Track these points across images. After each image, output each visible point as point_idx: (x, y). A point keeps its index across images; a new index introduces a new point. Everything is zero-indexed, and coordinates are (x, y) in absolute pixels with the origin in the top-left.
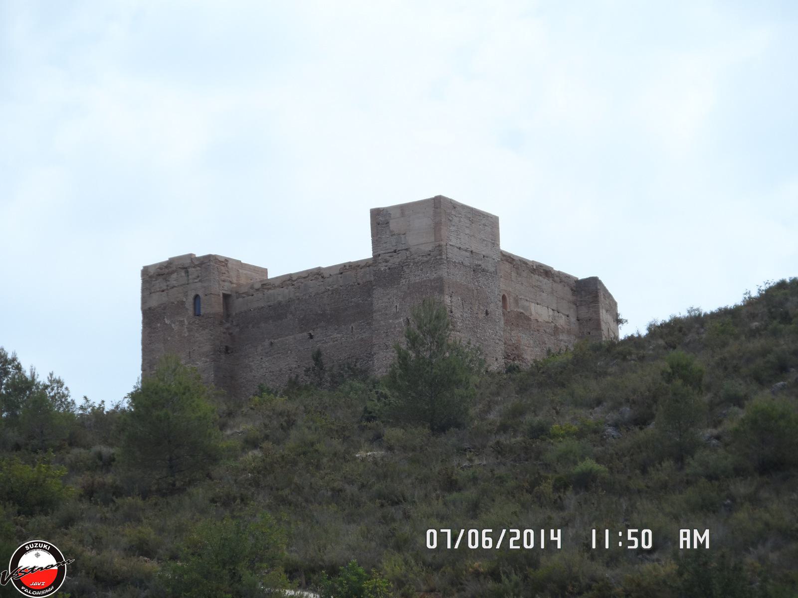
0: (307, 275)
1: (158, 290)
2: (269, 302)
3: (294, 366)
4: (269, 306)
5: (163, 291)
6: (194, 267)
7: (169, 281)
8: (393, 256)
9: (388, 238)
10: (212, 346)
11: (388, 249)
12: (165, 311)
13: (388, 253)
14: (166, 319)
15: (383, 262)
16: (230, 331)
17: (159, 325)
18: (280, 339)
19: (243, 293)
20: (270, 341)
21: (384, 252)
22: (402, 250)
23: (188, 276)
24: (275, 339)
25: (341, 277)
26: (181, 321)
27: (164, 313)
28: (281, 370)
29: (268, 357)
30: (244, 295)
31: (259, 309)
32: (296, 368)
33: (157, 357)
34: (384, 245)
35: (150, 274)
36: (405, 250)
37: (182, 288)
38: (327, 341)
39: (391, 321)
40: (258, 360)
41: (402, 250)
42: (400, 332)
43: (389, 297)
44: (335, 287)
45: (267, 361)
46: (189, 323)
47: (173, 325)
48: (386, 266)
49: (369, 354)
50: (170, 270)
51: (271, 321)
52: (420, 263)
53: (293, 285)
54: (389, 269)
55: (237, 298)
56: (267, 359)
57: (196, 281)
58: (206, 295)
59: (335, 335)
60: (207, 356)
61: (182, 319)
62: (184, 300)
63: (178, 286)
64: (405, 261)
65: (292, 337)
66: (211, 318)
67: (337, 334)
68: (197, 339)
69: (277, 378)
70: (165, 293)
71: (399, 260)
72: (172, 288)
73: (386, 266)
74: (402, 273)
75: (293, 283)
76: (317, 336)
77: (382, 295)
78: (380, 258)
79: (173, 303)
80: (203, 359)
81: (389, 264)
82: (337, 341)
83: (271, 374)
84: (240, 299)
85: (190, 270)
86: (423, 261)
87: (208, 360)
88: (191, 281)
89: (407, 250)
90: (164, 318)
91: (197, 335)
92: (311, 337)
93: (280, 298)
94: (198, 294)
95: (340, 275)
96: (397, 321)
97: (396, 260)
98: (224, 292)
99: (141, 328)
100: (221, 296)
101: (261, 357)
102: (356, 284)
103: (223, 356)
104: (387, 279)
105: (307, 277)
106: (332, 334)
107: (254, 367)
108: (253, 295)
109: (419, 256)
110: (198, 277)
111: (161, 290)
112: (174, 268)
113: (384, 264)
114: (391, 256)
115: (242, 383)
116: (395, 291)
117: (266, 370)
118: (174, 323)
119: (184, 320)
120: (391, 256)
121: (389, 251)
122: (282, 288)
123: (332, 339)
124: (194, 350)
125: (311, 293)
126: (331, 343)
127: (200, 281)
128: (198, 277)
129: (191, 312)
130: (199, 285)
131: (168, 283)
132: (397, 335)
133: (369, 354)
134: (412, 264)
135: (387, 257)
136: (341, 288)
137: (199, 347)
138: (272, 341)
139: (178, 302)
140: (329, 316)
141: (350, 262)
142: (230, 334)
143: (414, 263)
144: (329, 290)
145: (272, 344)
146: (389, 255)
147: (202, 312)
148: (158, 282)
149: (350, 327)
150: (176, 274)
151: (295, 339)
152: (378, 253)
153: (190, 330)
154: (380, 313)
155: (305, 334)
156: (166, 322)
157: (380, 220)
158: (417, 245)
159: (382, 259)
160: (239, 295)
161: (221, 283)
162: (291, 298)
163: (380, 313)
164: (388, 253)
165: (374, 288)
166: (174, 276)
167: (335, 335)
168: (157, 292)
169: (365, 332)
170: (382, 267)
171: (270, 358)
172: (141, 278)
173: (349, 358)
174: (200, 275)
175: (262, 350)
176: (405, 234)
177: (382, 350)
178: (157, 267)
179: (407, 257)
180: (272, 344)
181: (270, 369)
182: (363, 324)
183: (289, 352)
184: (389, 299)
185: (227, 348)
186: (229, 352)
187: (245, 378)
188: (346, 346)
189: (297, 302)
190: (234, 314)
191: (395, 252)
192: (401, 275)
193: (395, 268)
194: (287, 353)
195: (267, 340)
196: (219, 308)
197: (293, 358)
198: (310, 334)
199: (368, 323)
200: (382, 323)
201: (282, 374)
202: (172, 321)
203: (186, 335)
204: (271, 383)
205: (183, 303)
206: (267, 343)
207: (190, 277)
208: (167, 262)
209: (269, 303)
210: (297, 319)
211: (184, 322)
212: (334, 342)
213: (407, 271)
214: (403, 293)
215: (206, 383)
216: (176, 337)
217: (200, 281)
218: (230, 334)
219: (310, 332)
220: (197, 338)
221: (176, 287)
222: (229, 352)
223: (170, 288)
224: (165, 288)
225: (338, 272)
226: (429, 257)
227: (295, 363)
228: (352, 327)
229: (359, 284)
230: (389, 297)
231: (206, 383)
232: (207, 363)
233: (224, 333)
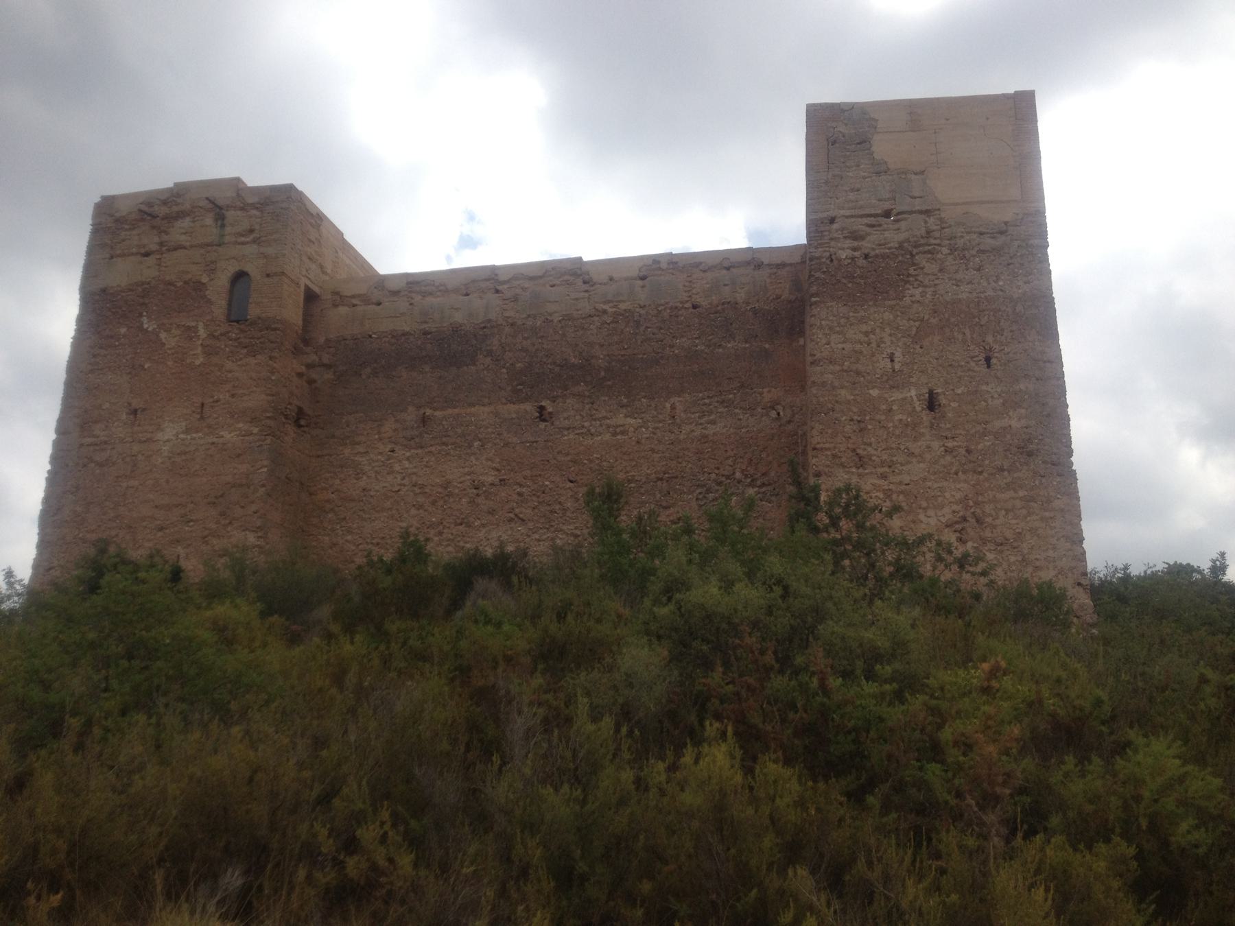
0: (540, 274)
1: (134, 250)
2: (426, 322)
3: (490, 479)
4: (426, 333)
5: (147, 255)
6: (242, 209)
7: (166, 233)
8: (880, 225)
9: (864, 178)
10: (270, 398)
11: (861, 207)
12: (147, 301)
13: (862, 216)
14: (145, 320)
15: (845, 237)
16: (314, 376)
17: (123, 330)
18: (450, 411)
19: (353, 297)
20: (422, 412)
21: (848, 213)
22: (911, 212)
23: (223, 226)
24: (435, 409)
25: (643, 287)
26: (189, 328)
27: (143, 304)
28: (446, 485)
29: (410, 448)
30: (355, 301)
31: (393, 337)
32: (492, 484)
33: (107, 405)
34: (852, 196)
35: (118, 215)
36: (921, 212)
37: (202, 251)
38: (593, 430)
39: (875, 393)
40: (381, 453)
41: (911, 212)
42: (907, 425)
43: (864, 328)
44: (623, 306)
45: (408, 459)
46: (212, 336)
47: (163, 335)
48: (854, 249)
49: (728, 477)
50: (175, 209)
51: (427, 368)
52: (974, 252)
53: (497, 291)
54: (866, 256)
55: (335, 306)
56: (408, 454)
57: (243, 239)
58: (268, 275)
59: (620, 419)
60: (253, 420)
61: (193, 324)
62: (205, 279)
63: (191, 246)
64: (922, 241)
65: (486, 409)
66: (275, 329)
67: (626, 416)
68: (230, 375)
69: (434, 503)
70: (151, 260)
71: (902, 236)
72: (175, 249)
73: (854, 249)
74: (912, 271)
75: (499, 288)
76: (565, 415)
77: (843, 321)
78: (835, 226)
79: (170, 283)
80: (241, 425)
81: (866, 245)
82: (622, 433)
83: (418, 491)
84: (343, 310)
85: (230, 215)
86: (982, 247)
87: (255, 430)
88: (227, 239)
89: (927, 212)
90: (141, 315)
91: (229, 365)
92: (542, 414)
93: (458, 318)
94: (246, 269)
95: (640, 283)
96: (897, 395)
97: (892, 235)
98: (309, 283)
99: (72, 333)
100: (303, 288)
101: (390, 447)
102: (688, 305)
103: (290, 429)
104: (859, 280)
105: (541, 277)
106: (609, 415)
107: (367, 468)
108: (379, 304)
109: (968, 233)
110: (252, 231)
111: (143, 251)
112: (187, 206)
113: (849, 243)
114: (872, 226)
115: (328, 501)
116: (888, 316)
117: (403, 478)
118: (168, 331)
119: (196, 327)
120: (872, 226)
121: (867, 211)
122: (467, 295)
123: (609, 427)
124: (217, 401)
125: (551, 314)
126: (607, 437)
127: (254, 241)
128: (252, 231)
129: (219, 308)
130: (250, 250)
131: (165, 237)
132: (897, 432)
133: (728, 477)
134: (945, 250)
135: (860, 225)
136: (642, 312)
137: (233, 396)
138: (429, 412)
139: (185, 283)
140: (603, 374)
141: (671, 254)
142: (311, 382)
143: (953, 250)
144: (605, 312)
145: (424, 420)
146: (866, 221)
147: (254, 312)
148: (134, 232)
149: (668, 405)
150: (188, 219)
151: (497, 414)
152: (832, 213)
153: (209, 352)
154: (838, 368)
155: (528, 407)
156: (145, 326)
157: (839, 138)
158: (964, 204)
159: (843, 229)
160: (339, 298)
161: (304, 258)
162: (489, 321)
163: (838, 368)
164: (862, 216)
165: (816, 302)
166: (186, 223)
167: (620, 419)
168: (133, 254)
169: (713, 422)
170: (843, 249)
171: (420, 451)
172: (90, 222)
173: (661, 479)
174: (257, 227)
175: (395, 430)
176: (922, 172)
177: (844, 467)
178: (141, 200)
179: (929, 232)
180: (424, 420)
181: (414, 478)
182: (707, 401)
183: (476, 444)
184: (867, 334)
185: (300, 412)
186: (302, 422)
187: (338, 490)
188: (652, 450)
189: (507, 330)
190: (322, 340)
191: (887, 214)
192: (909, 275)
193: (884, 256)
194: (470, 446)
195: (411, 409)
196: (293, 313)
197: (488, 460)
198: (542, 408)
199: (723, 402)
200: (844, 394)
201: (450, 495)
202: (163, 324)
203: (197, 362)
204: (413, 512)
205: (199, 287)
206: (411, 415)
207: (228, 229)
208: (171, 189)
209: (425, 326)
210: (504, 370)
211: (196, 332)
212: (615, 434)
213: (931, 268)
214: (917, 324)
215: (241, 485)
216: (170, 363)
217: (254, 241)
218: (311, 382)
219: (543, 404)
220: (230, 371)
221: (185, 248)
222: (302, 422)
223: (168, 250)
224: (154, 247)
225: (635, 273)
226: (1002, 239)
227: (493, 473)
228: (673, 408)
229: (695, 307)
230: (864, 328)
231: (241, 485)
232: (251, 438)
233: (300, 375)
